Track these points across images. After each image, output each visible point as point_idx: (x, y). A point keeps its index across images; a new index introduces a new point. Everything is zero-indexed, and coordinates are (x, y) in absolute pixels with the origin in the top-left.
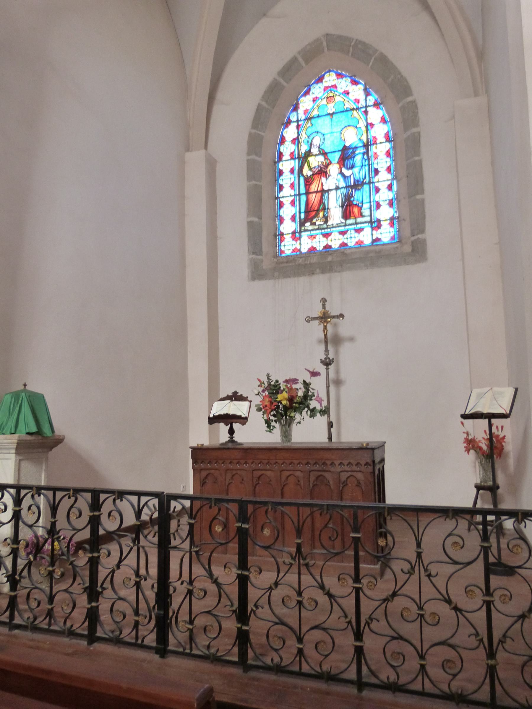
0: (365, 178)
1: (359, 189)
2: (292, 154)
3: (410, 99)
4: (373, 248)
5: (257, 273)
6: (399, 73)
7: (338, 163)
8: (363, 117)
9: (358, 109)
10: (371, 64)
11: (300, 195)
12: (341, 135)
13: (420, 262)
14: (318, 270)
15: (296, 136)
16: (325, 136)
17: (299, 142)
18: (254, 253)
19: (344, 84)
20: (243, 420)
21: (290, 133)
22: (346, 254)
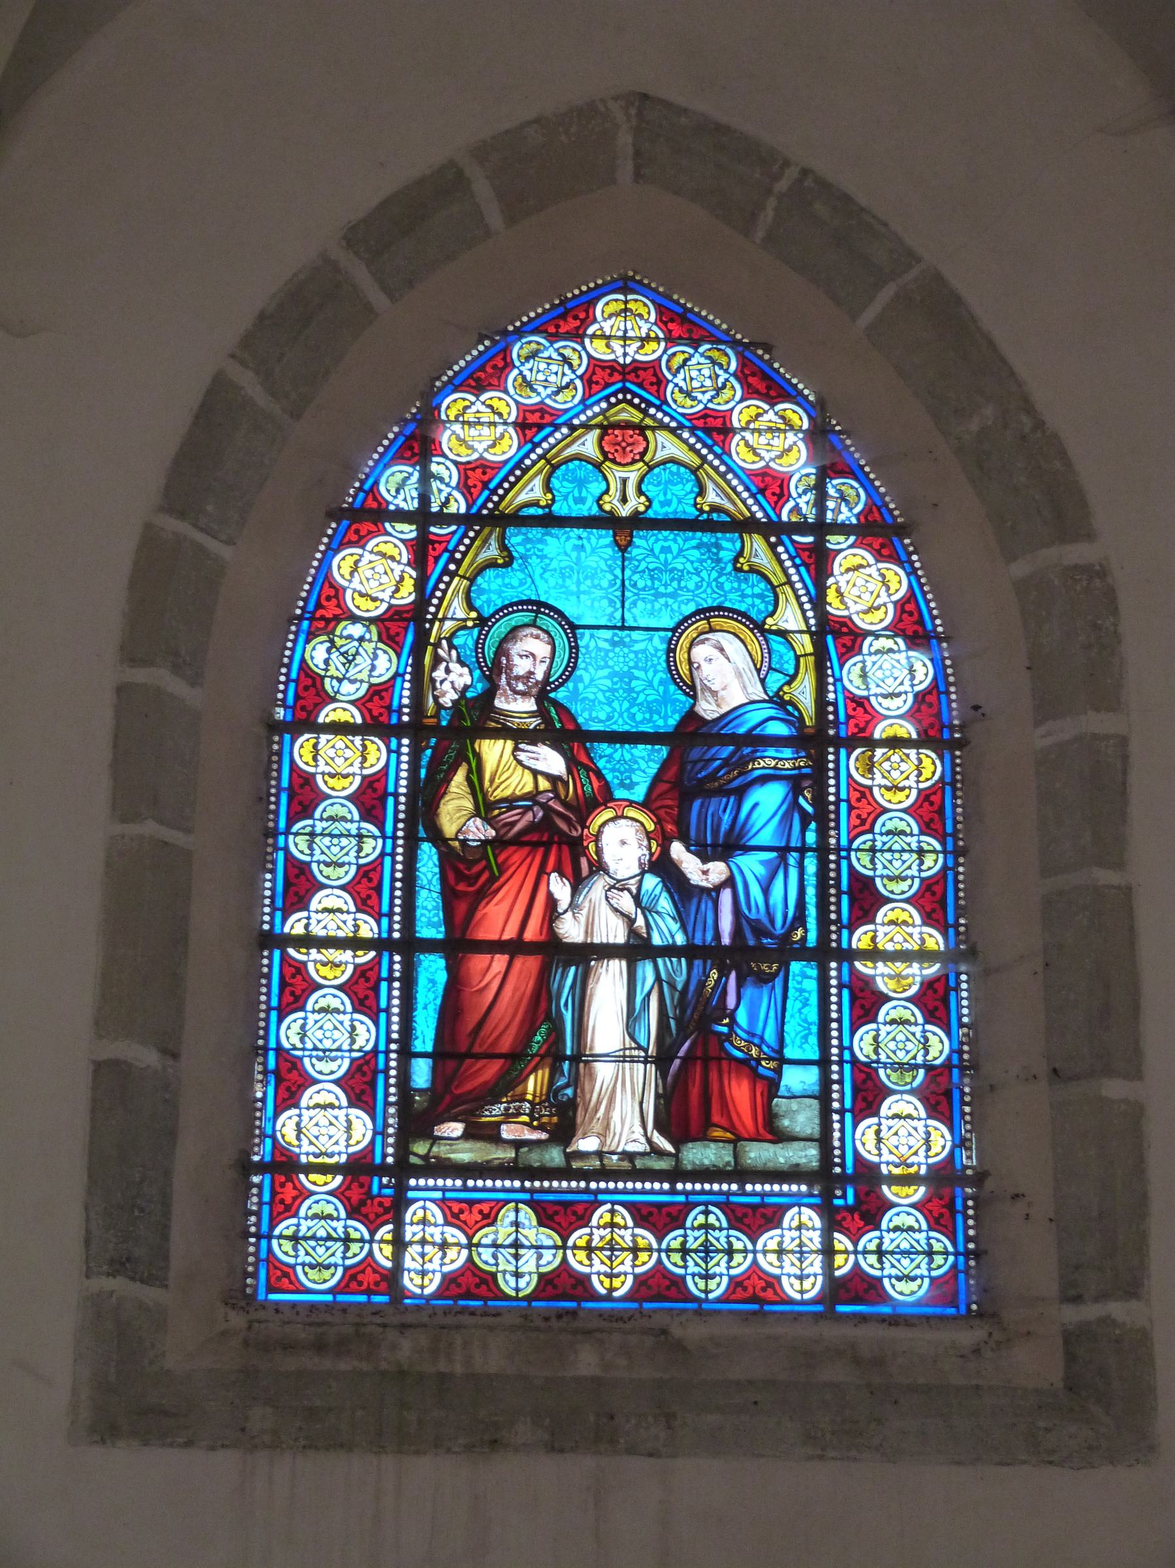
0: (800, 918)
1: (764, 979)
3: (1077, 553)
4: (831, 1332)
5: (129, 1403)
6: (1028, 407)
7: (646, 805)
10: (868, 316)
11: (410, 946)
12: (671, 651)
18: (120, 1266)
19: (700, 377)
21: (374, 574)
22: (679, 1347)
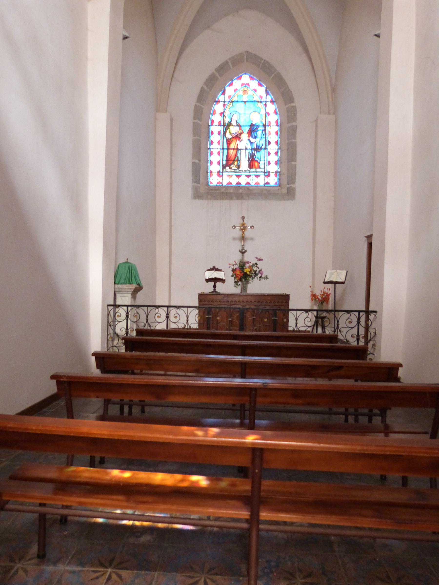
1: (259, 152)
2: (220, 122)
3: (293, 105)
5: (197, 195)
6: (288, 87)
8: (264, 107)
9: (261, 102)
11: (223, 149)
13: (291, 200)
14: (234, 198)
15: (223, 111)
16: (241, 115)
17: (224, 116)
18: (196, 182)
19: (254, 84)
20: (223, 281)
21: (218, 108)
